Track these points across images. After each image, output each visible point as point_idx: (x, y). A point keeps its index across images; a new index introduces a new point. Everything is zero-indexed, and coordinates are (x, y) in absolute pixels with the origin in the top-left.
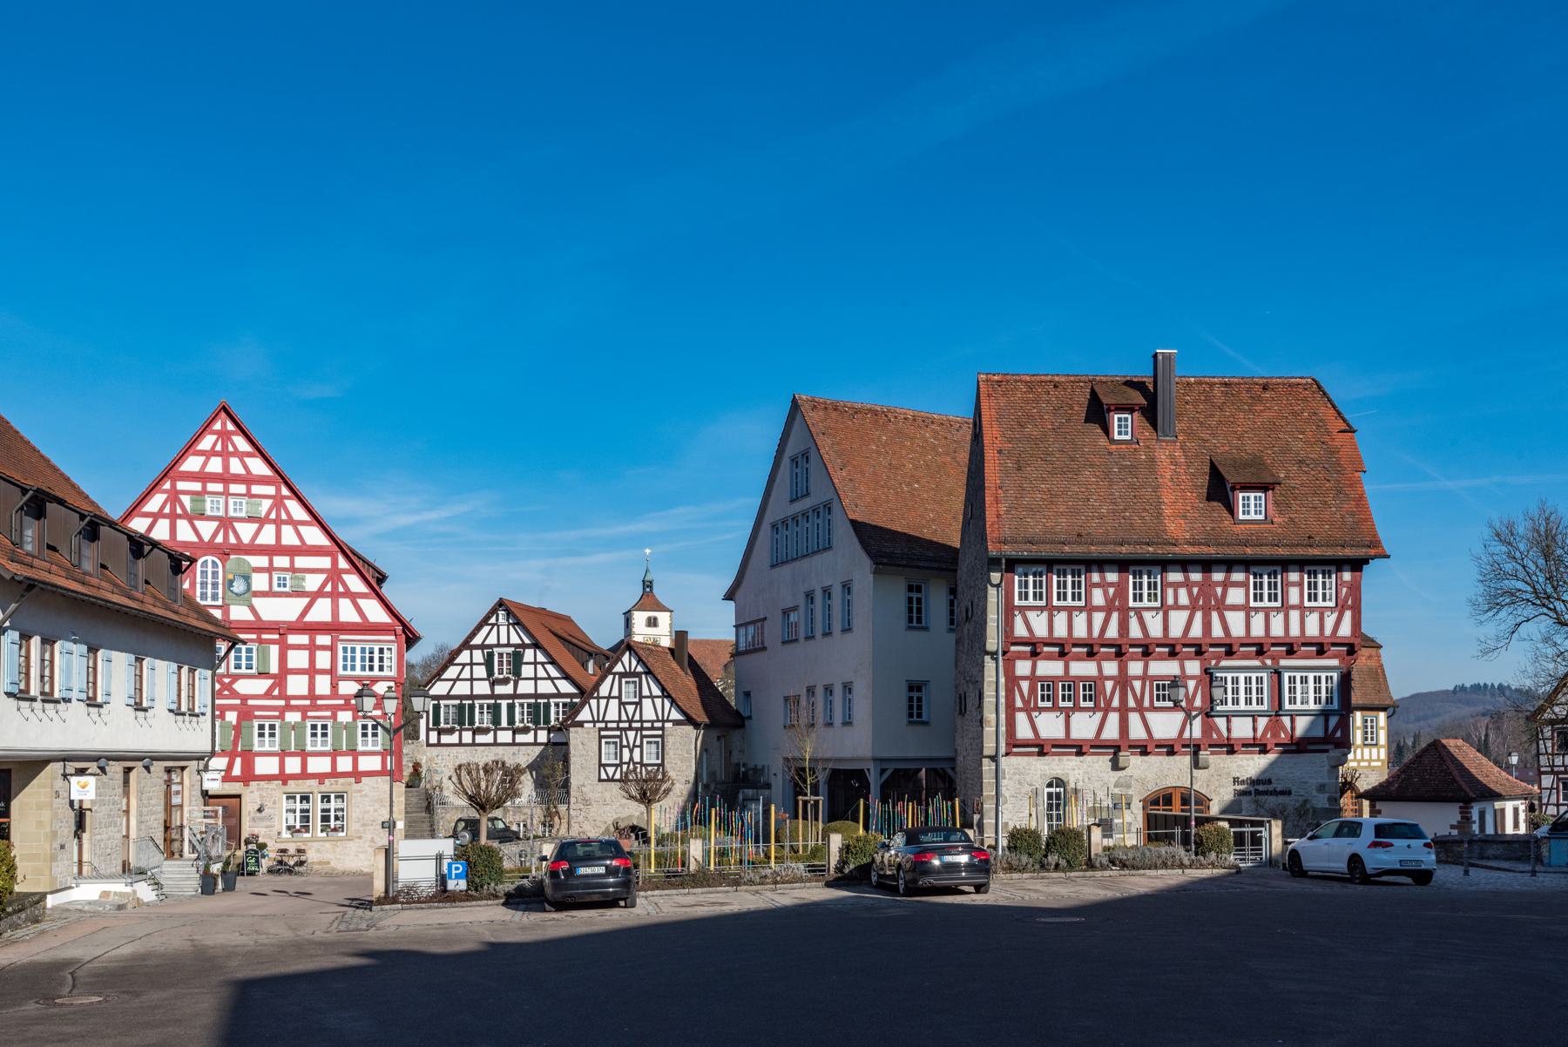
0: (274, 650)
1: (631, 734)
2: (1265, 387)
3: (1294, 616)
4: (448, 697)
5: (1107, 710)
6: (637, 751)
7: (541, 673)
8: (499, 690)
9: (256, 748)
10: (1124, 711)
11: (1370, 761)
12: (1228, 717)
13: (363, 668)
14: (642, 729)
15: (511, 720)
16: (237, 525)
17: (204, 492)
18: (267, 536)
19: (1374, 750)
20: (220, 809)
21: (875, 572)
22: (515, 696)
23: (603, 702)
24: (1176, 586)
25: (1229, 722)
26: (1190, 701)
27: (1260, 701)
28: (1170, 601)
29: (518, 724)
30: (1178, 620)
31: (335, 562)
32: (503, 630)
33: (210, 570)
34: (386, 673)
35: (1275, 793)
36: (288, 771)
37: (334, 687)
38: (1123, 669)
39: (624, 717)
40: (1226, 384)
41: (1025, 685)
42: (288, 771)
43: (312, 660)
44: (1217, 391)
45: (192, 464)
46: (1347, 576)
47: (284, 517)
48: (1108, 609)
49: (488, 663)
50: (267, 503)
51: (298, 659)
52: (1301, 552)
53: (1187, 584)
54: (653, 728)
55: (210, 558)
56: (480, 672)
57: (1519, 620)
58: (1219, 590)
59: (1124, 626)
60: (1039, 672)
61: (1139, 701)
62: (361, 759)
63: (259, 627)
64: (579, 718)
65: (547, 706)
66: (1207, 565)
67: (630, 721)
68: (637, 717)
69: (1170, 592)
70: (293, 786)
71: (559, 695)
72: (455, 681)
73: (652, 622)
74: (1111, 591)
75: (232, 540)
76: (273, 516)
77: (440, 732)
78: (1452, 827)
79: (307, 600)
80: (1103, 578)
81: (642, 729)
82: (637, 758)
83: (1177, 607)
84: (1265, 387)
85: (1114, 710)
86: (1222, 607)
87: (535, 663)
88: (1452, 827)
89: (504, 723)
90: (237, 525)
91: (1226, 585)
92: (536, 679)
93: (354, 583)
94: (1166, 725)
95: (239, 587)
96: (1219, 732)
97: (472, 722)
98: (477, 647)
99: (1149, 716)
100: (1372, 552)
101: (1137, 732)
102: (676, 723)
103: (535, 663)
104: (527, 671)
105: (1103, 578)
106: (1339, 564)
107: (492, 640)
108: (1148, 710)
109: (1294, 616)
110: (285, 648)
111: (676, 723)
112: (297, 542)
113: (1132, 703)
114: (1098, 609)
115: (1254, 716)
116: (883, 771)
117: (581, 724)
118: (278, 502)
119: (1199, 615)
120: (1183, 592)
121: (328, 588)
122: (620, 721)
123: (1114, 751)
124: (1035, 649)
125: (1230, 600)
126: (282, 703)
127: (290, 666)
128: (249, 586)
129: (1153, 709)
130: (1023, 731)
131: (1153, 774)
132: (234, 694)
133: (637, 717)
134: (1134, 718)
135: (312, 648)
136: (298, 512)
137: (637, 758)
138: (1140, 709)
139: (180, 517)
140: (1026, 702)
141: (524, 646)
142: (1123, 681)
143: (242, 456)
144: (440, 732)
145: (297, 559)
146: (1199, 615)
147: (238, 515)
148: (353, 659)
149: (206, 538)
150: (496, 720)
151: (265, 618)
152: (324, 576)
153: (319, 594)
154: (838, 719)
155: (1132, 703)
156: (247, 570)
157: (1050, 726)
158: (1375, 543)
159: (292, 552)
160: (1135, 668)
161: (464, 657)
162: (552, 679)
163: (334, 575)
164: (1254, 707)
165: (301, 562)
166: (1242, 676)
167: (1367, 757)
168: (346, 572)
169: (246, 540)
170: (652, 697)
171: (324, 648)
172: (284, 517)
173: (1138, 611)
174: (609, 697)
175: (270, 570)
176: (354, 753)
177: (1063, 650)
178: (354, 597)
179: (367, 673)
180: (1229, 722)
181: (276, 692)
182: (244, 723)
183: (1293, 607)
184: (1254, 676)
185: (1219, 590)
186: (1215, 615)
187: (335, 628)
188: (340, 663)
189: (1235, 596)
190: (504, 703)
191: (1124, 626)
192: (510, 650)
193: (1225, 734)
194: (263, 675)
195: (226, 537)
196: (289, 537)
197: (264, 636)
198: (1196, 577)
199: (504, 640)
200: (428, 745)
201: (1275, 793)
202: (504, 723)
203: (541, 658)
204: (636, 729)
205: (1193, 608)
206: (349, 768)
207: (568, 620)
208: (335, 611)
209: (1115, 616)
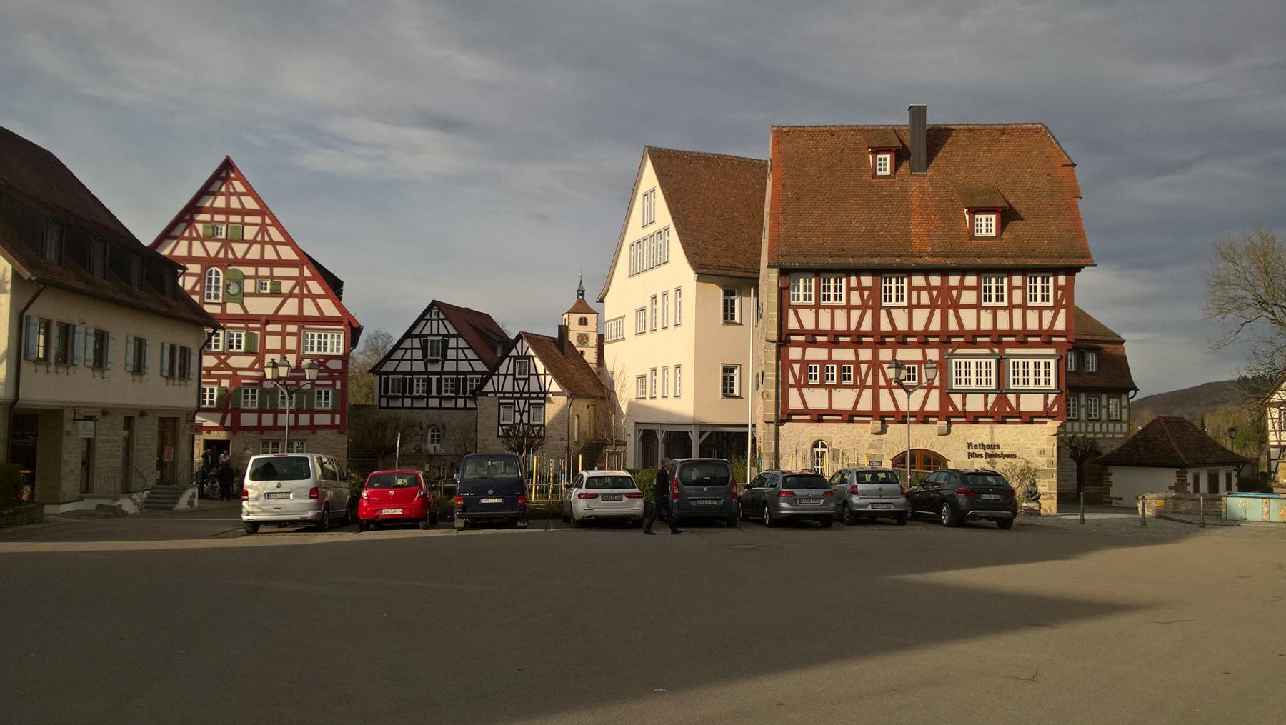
1: (522, 402)
2: (1003, 132)
3: (1017, 313)
4: (395, 372)
5: (863, 386)
6: (526, 415)
7: (461, 356)
8: (431, 368)
9: (242, 406)
10: (876, 388)
11: (1114, 433)
12: (964, 393)
13: (319, 349)
14: (530, 398)
15: (439, 390)
16: (234, 245)
17: (244, 224)
18: (254, 253)
21: (698, 280)
22: (442, 372)
23: (502, 378)
24: (919, 289)
25: (964, 398)
26: (863, 381)
27: (988, 382)
28: (914, 302)
29: (444, 394)
30: (920, 317)
31: (302, 272)
32: (435, 323)
33: (214, 277)
34: (335, 353)
35: (1002, 456)
36: (264, 424)
38: (875, 354)
40: (970, 130)
41: (797, 367)
42: (264, 424)
43: (283, 343)
46: (1062, 280)
47: (267, 239)
48: (863, 307)
49: (424, 348)
52: (1022, 261)
53: (929, 288)
54: (537, 398)
55: (214, 269)
56: (418, 354)
57: (1243, 321)
59: (876, 321)
61: (888, 381)
62: (316, 416)
63: (246, 318)
64: (485, 389)
65: (465, 380)
66: (944, 272)
67: (521, 392)
69: (914, 294)
70: (267, 435)
71: (473, 372)
72: (399, 361)
73: (583, 322)
74: (866, 293)
75: (230, 256)
76: (259, 238)
77: (389, 398)
78: (1171, 488)
79: (280, 300)
80: (859, 282)
81: (530, 398)
82: (525, 421)
83: (919, 306)
84: (1003, 132)
85: (869, 387)
86: (957, 306)
87: (457, 348)
88: (1171, 488)
89: (434, 393)
90: (234, 245)
91: (962, 287)
92: (457, 360)
93: (315, 287)
94: (913, 402)
95: (234, 289)
96: (955, 407)
97: (411, 392)
98: (416, 336)
100: (1083, 262)
101: (886, 404)
103: (457, 348)
105: (859, 282)
106: (1055, 271)
107: (426, 331)
109: (1017, 313)
110: (265, 334)
112: (275, 257)
113: (882, 382)
114: (856, 307)
115: (986, 393)
116: (702, 434)
117: (486, 394)
118: (263, 228)
119: (938, 312)
120: (924, 294)
121: (296, 291)
122: (514, 392)
123: (883, 418)
124: (811, 339)
125: (963, 301)
127: (268, 347)
129: (807, 386)
130: (795, 402)
131: (899, 439)
132: (228, 367)
134: (884, 394)
135: (284, 334)
136: (277, 237)
137: (525, 421)
138: (889, 387)
139: (195, 239)
142: (876, 364)
143: (239, 195)
144: (389, 398)
146: (938, 312)
148: (319, 343)
149: (212, 255)
150: (429, 391)
151: (251, 312)
153: (291, 295)
154: (671, 394)
155: (882, 382)
156: (240, 278)
157: (817, 399)
158: (1086, 255)
159: (271, 264)
161: (407, 344)
162: (467, 359)
163: (301, 281)
164: (984, 386)
165: (278, 271)
166: (973, 362)
167: (1111, 430)
168: (309, 279)
169: (240, 256)
172: (267, 239)
173: (888, 310)
174: (506, 375)
175: (256, 277)
176: (276, 412)
177: (834, 340)
178: (314, 297)
179: (322, 353)
180: (964, 398)
183: (1017, 306)
184: (983, 361)
185: (955, 293)
186: (951, 312)
187: (301, 320)
189: (969, 297)
190: (434, 378)
191: (876, 321)
193: (960, 408)
195: (226, 253)
196: (270, 254)
198: (935, 280)
199: (435, 332)
201: (1002, 456)
202: (434, 393)
204: (526, 399)
205: (932, 307)
206: (307, 423)
207: (487, 317)
209: (869, 313)
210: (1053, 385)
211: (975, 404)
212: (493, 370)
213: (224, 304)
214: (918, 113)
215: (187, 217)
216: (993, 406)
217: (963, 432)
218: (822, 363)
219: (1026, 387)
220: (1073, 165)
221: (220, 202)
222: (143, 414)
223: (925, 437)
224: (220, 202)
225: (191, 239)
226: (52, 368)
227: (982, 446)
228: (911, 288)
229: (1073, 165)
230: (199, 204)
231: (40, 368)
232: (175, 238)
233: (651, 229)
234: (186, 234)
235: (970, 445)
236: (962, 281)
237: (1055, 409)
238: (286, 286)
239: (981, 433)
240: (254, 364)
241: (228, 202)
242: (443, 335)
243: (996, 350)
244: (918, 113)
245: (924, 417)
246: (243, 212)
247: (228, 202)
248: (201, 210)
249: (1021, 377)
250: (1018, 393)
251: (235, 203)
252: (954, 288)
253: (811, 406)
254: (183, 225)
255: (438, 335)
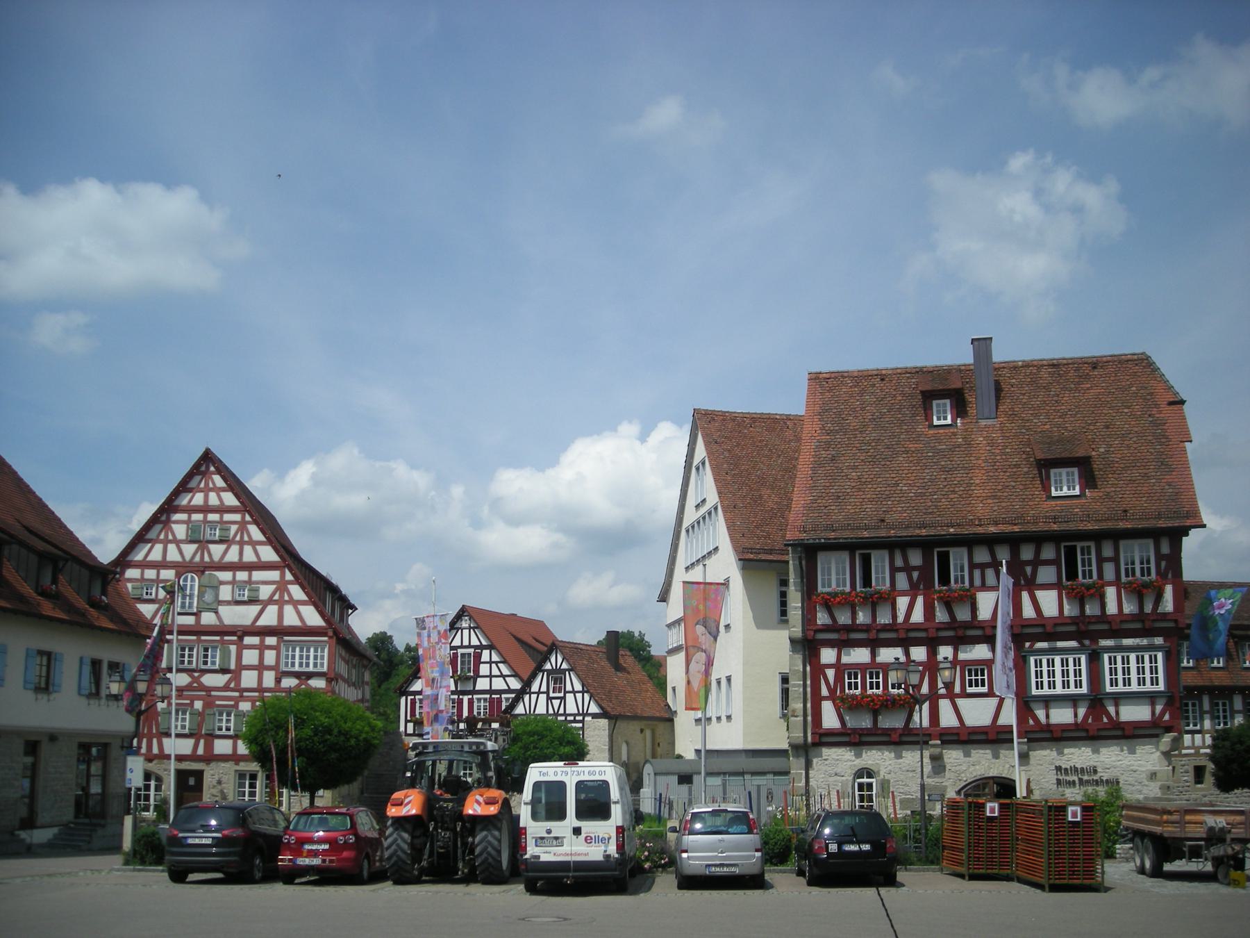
0: (233, 648)
7: (495, 672)
18: (233, 556)
19: (1198, 737)
20: (996, 805)
24: (983, 567)
27: (1078, 684)
34: (319, 669)
37: (278, 681)
39: (551, 711)
40: (1054, 365)
41: (830, 673)
44: (1044, 373)
45: (184, 500)
50: (234, 528)
51: (250, 657)
55: (189, 575)
58: (1029, 570)
60: (162, 577)
61: (949, 686)
65: (500, 701)
68: (561, 711)
69: (977, 573)
74: (915, 575)
75: (207, 559)
76: (238, 538)
79: (258, 608)
87: (490, 662)
92: (491, 676)
94: (977, 713)
95: (208, 597)
99: (960, 702)
100: (1188, 523)
101: (948, 719)
102: (595, 716)
103: (490, 662)
104: (484, 669)
108: (959, 696)
110: (241, 648)
111: (595, 716)
118: (243, 526)
121: (276, 597)
126: (237, 694)
128: (217, 595)
133: (561, 711)
134: (944, 704)
135: (262, 648)
138: (952, 696)
139: (171, 542)
140: (832, 691)
141: (482, 647)
142: (932, 667)
145: (254, 573)
147: (212, 538)
149: (188, 558)
152: (274, 587)
153: (270, 601)
156: (216, 584)
159: (250, 567)
160: (945, 652)
162: (502, 676)
163: (282, 586)
168: (291, 583)
170: (574, 692)
171: (270, 647)
172: (246, 538)
174: (539, 693)
175: (233, 582)
178: (296, 604)
179: (304, 669)
181: (232, 685)
182: (208, 711)
185: (1029, 570)
187: (279, 631)
188: (283, 660)
192: (471, 651)
194: (224, 671)
196: (249, 556)
197: (226, 638)
199: (466, 643)
200: (407, 735)
203: (495, 658)
208: (281, 616)
209: (920, 601)
210: (1161, 687)
211: (1062, 716)
212: (525, 689)
213: (197, 615)
214: (982, 345)
215: (164, 518)
216: (1086, 717)
217: (1045, 757)
218: (862, 667)
219: (1127, 689)
220: (1182, 402)
221: (198, 499)
222: (53, 737)
223: (1005, 764)
224: (198, 499)
225: (166, 542)
226: (103, 701)
227: (1075, 770)
228: (972, 566)
229: (1182, 402)
230: (176, 503)
231: (92, 702)
232: (149, 541)
233: (703, 510)
234: (162, 537)
235: (1058, 769)
236: (1038, 552)
237: (1167, 717)
238: (265, 592)
239: (1079, 756)
240: (229, 682)
241: (206, 498)
242: (475, 647)
243: (1087, 642)
244: (982, 345)
245: (994, 737)
246: (222, 510)
247: (206, 498)
248: (177, 510)
249: (1120, 676)
250: (1118, 698)
251: (213, 499)
252: (1028, 563)
253: (970, 721)
254: (158, 527)
255: (470, 646)
